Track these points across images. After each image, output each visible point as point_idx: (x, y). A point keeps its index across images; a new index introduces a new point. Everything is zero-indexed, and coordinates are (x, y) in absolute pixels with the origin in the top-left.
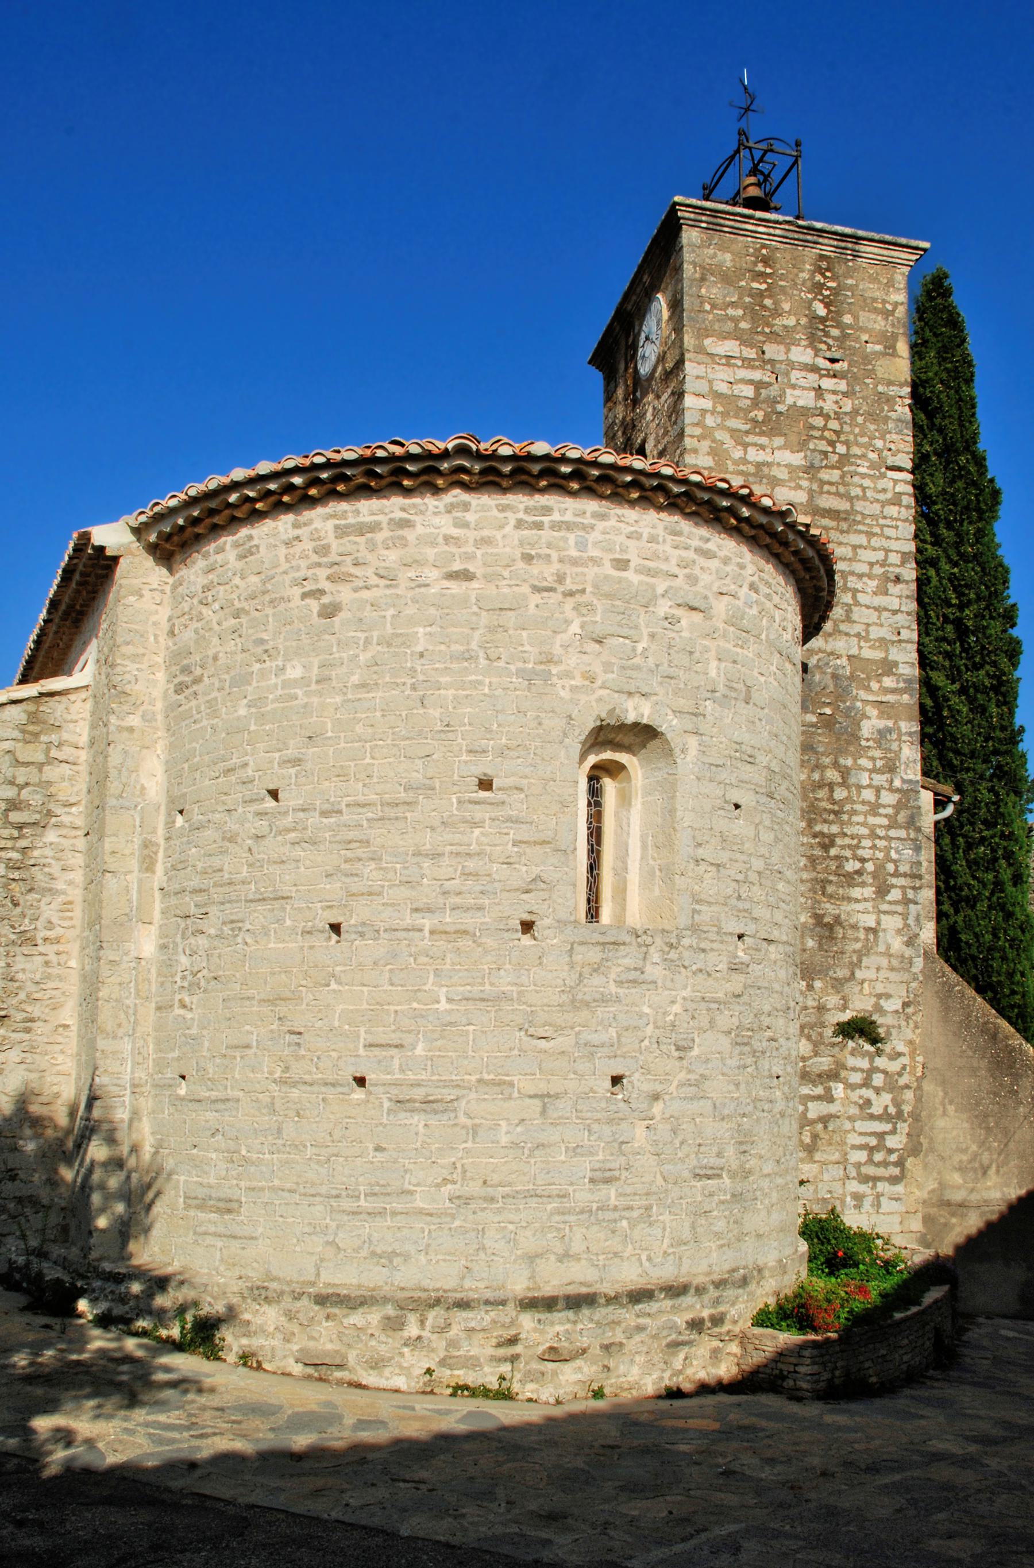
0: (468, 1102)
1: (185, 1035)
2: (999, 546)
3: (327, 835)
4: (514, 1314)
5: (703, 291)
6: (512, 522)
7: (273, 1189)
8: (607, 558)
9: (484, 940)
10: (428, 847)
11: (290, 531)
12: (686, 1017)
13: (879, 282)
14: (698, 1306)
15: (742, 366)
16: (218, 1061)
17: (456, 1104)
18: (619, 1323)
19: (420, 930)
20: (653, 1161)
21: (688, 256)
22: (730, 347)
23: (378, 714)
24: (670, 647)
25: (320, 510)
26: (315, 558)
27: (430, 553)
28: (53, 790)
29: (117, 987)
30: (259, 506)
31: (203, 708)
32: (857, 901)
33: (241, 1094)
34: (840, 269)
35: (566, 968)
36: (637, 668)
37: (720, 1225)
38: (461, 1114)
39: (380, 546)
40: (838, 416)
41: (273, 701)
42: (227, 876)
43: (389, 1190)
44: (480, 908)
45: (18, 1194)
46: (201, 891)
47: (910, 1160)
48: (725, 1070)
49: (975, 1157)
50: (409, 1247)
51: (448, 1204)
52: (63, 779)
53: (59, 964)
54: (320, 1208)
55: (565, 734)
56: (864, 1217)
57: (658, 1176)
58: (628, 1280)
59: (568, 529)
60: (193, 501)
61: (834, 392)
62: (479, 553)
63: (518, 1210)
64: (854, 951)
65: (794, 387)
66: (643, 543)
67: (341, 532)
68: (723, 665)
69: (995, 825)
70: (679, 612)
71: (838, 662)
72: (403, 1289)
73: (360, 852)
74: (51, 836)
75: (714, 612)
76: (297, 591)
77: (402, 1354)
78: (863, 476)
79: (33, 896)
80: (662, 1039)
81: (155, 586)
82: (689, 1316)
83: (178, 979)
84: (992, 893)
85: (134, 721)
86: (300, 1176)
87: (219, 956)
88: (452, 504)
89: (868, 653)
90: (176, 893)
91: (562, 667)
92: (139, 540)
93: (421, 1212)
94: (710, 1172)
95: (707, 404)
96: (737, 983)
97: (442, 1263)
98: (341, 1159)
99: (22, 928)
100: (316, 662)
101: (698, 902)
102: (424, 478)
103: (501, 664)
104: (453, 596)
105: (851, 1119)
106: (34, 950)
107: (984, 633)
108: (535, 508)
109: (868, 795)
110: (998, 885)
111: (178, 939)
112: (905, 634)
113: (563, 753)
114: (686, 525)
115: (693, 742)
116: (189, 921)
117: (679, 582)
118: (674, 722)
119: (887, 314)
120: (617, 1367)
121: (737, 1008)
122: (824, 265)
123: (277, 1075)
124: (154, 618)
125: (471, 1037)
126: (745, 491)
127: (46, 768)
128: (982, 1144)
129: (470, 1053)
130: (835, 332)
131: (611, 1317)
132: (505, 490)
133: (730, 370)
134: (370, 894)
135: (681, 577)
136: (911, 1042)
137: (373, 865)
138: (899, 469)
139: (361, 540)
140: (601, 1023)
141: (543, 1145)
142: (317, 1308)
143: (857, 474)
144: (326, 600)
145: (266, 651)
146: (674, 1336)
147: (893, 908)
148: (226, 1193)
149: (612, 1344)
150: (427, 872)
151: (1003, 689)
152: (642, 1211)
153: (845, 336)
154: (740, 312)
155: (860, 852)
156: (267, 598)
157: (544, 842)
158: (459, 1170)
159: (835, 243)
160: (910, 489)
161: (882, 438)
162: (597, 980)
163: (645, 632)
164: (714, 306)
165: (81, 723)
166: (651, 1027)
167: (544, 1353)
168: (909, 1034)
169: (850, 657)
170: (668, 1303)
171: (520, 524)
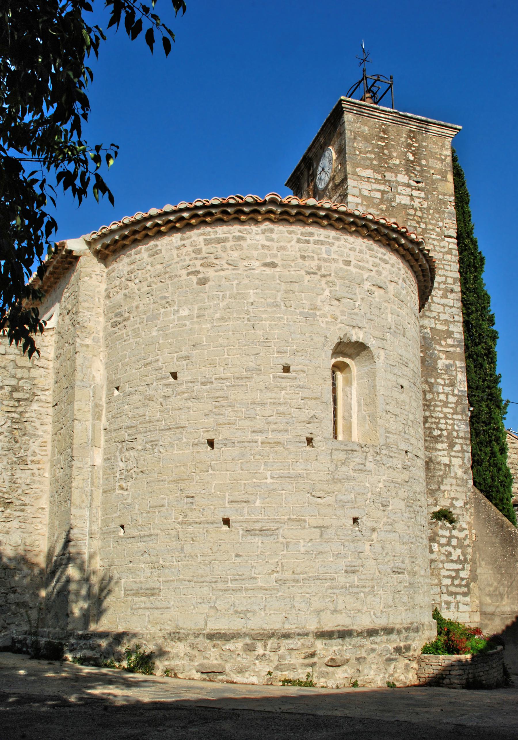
0: (283, 530)
1: (123, 504)
2: (485, 285)
3: (205, 394)
4: (313, 640)
5: (355, 144)
6: (295, 240)
7: (179, 580)
8: (340, 259)
9: (288, 447)
10: (259, 400)
11: (179, 242)
12: (385, 490)
13: (438, 145)
14: (398, 640)
15: (375, 183)
16: (144, 515)
17: (277, 531)
18: (363, 647)
19: (256, 442)
20: (374, 562)
21: (347, 127)
22: (369, 173)
23: (231, 333)
24: (371, 305)
25: (196, 231)
26: (194, 255)
27: (255, 253)
28: (36, 382)
29: (82, 481)
30: (162, 229)
31: (130, 333)
32: (440, 450)
33: (159, 531)
34: (419, 138)
35: (329, 462)
36: (356, 314)
37: (405, 599)
38: (280, 536)
39: (229, 249)
40: (421, 210)
41: (172, 328)
42: (147, 418)
43: (244, 577)
44: (286, 431)
45: (17, 601)
46: (131, 427)
47: (472, 584)
48: (403, 519)
49: (496, 589)
50: (256, 608)
51: (275, 584)
52: (41, 376)
53: (39, 475)
54: (206, 588)
55: (324, 346)
56: (451, 613)
57: (377, 571)
58: (365, 624)
59: (322, 244)
60: (126, 226)
61: (419, 198)
62: (279, 254)
63: (310, 586)
64: (439, 476)
65: (400, 194)
66: (356, 253)
67: (208, 242)
68: (394, 316)
69: (490, 424)
70: (374, 288)
71: (426, 330)
72: (253, 630)
73: (223, 403)
74: (35, 406)
75: (389, 290)
76: (185, 272)
77: (255, 664)
78: (434, 239)
79: (25, 438)
80: (375, 500)
81: (98, 273)
82: (395, 645)
83: (117, 475)
84: (490, 458)
85: (89, 341)
86: (194, 573)
87: (144, 460)
88: (265, 229)
89: (439, 327)
90: (115, 430)
91: (322, 312)
92: (90, 249)
93: (261, 588)
94: (399, 571)
95: (359, 200)
96: (405, 475)
97: (273, 615)
98: (217, 562)
99: (20, 455)
100: (196, 307)
101: (388, 432)
102: (251, 216)
103: (292, 309)
104: (267, 275)
105: (442, 562)
106: (26, 467)
107: (480, 328)
108: (306, 233)
109: (442, 397)
110: (493, 453)
111: (118, 454)
112: (457, 318)
113: (323, 354)
114: (375, 246)
115: (382, 353)
116: (124, 444)
117: (373, 274)
118: (374, 342)
119: (442, 161)
120: (363, 670)
121: (407, 488)
122: (412, 135)
123: (180, 520)
124: (98, 289)
125: (284, 497)
126: (404, 230)
127: (32, 370)
128: (499, 582)
129: (284, 505)
130: (418, 168)
131: (359, 643)
132: (291, 224)
133: (369, 184)
134: (229, 424)
135: (374, 271)
136: (469, 523)
137: (230, 409)
138: (450, 237)
139: (219, 246)
140: (347, 490)
141: (322, 552)
142: (208, 641)
143: (431, 238)
144: (200, 276)
145: (168, 302)
146: (388, 655)
147: (457, 454)
148: (151, 585)
149: (361, 658)
150: (259, 412)
151: (491, 356)
152: (370, 588)
153: (422, 171)
154: (373, 156)
155: (440, 426)
156: (167, 275)
157: (316, 398)
158: (280, 566)
159: (417, 124)
160: (456, 247)
161: (442, 221)
162: (344, 468)
163: (359, 297)
164: (360, 152)
165: (50, 347)
166: (370, 494)
167: (328, 661)
168: (468, 518)
169: (431, 329)
170: (385, 637)
171: (298, 241)
